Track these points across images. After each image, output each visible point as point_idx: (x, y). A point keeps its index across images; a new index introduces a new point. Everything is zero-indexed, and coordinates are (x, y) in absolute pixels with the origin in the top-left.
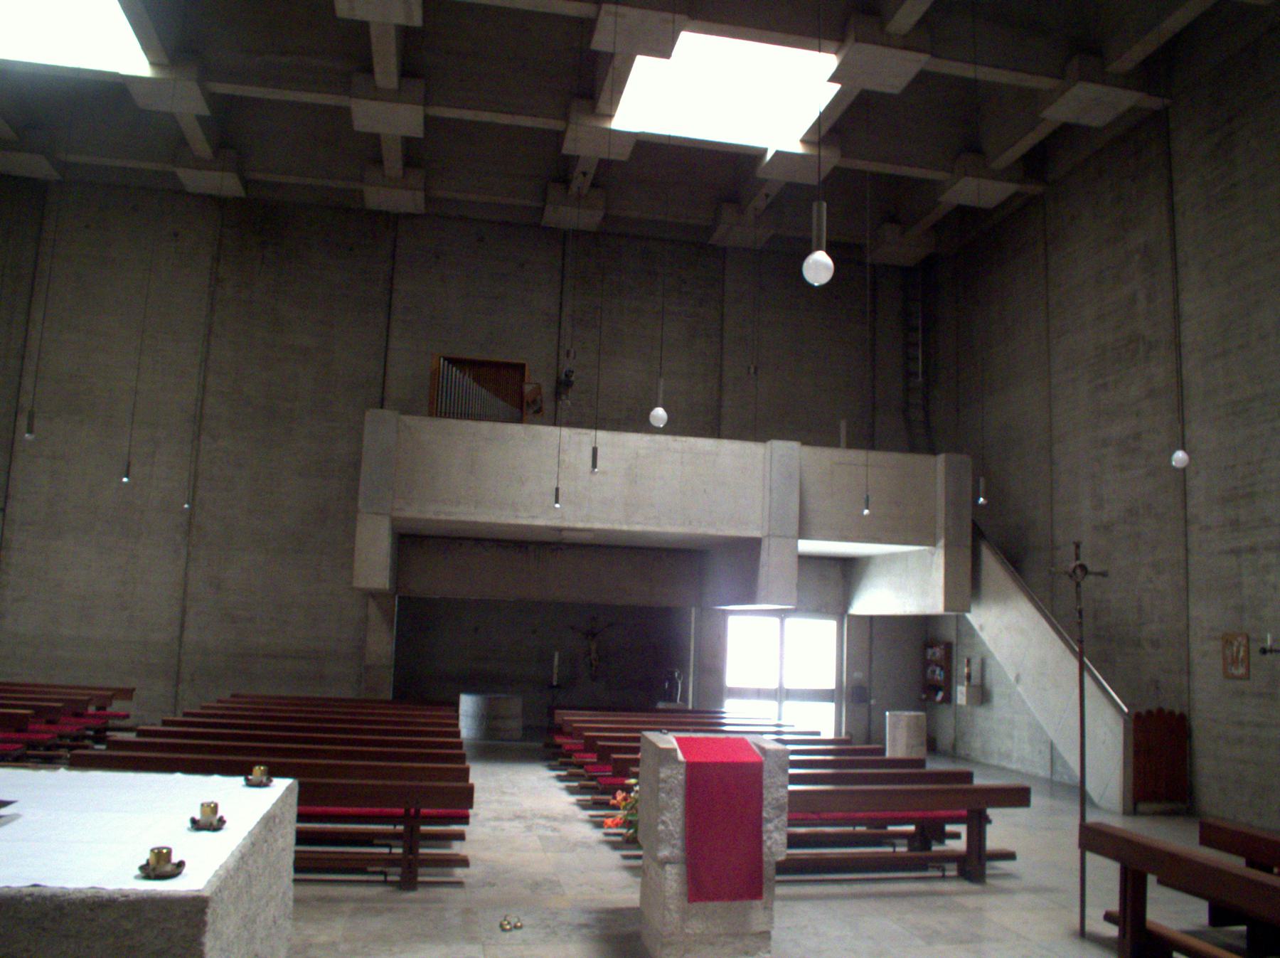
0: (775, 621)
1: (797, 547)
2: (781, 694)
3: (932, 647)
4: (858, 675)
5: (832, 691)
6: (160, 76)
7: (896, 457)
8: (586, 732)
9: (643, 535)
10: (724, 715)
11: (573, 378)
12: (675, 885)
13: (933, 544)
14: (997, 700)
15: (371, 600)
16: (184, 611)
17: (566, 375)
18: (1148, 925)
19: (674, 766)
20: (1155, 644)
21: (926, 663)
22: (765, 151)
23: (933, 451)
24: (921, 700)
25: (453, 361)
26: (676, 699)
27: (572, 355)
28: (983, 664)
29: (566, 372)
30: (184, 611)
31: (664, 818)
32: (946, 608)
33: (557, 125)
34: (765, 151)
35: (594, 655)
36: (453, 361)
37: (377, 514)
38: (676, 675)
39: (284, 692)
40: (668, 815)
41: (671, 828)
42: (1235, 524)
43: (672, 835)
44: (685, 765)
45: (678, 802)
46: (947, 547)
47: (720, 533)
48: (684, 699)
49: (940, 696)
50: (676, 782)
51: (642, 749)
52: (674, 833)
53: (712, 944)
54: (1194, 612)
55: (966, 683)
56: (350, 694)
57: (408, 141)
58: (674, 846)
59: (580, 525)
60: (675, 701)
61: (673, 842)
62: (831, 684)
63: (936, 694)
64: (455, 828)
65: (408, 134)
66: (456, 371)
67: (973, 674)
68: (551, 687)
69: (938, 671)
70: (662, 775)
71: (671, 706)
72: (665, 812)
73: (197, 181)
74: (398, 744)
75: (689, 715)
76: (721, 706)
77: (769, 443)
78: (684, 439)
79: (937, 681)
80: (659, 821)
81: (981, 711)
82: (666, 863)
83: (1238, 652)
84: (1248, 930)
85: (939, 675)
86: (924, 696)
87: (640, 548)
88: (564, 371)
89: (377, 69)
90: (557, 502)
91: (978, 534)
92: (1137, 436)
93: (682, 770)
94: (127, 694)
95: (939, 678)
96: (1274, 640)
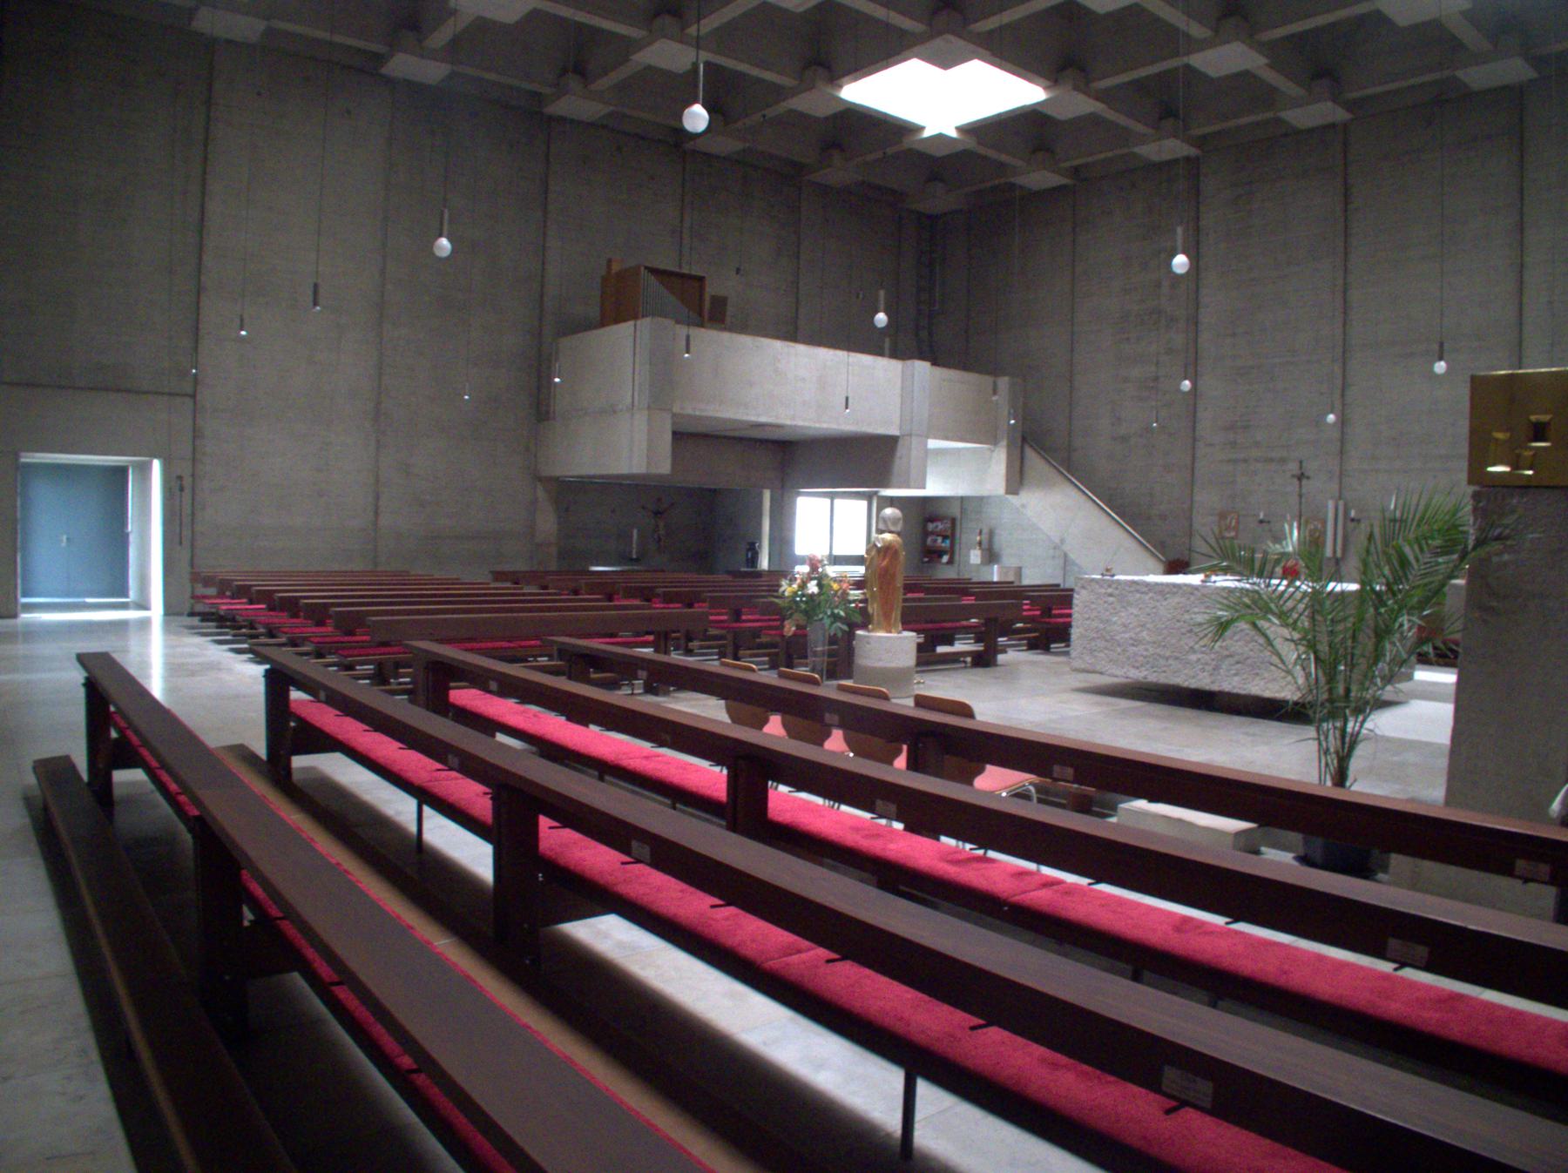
0: (828, 501)
8: (246, 648)
13: (993, 440)
15: (538, 483)
16: (377, 498)
20: (1163, 517)
21: (926, 534)
22: (922, 128)
24: (923, 563)
28: (991, 534)
30: (377, 498)
34: (922, 128)
35: (662, 532)
37: (661, 409)
42: (1233, 444)
49: (945, 559)
51: (901, 601)
54: (1197, 498)
55: (978, 548)
64: (1066, 611)
77: (909, 362)
83: (1231, 522)
84: (1468, 583)
86: (926, 559)
91: (1024, 440)
92: (1156, 379)
96: (1265, 515)
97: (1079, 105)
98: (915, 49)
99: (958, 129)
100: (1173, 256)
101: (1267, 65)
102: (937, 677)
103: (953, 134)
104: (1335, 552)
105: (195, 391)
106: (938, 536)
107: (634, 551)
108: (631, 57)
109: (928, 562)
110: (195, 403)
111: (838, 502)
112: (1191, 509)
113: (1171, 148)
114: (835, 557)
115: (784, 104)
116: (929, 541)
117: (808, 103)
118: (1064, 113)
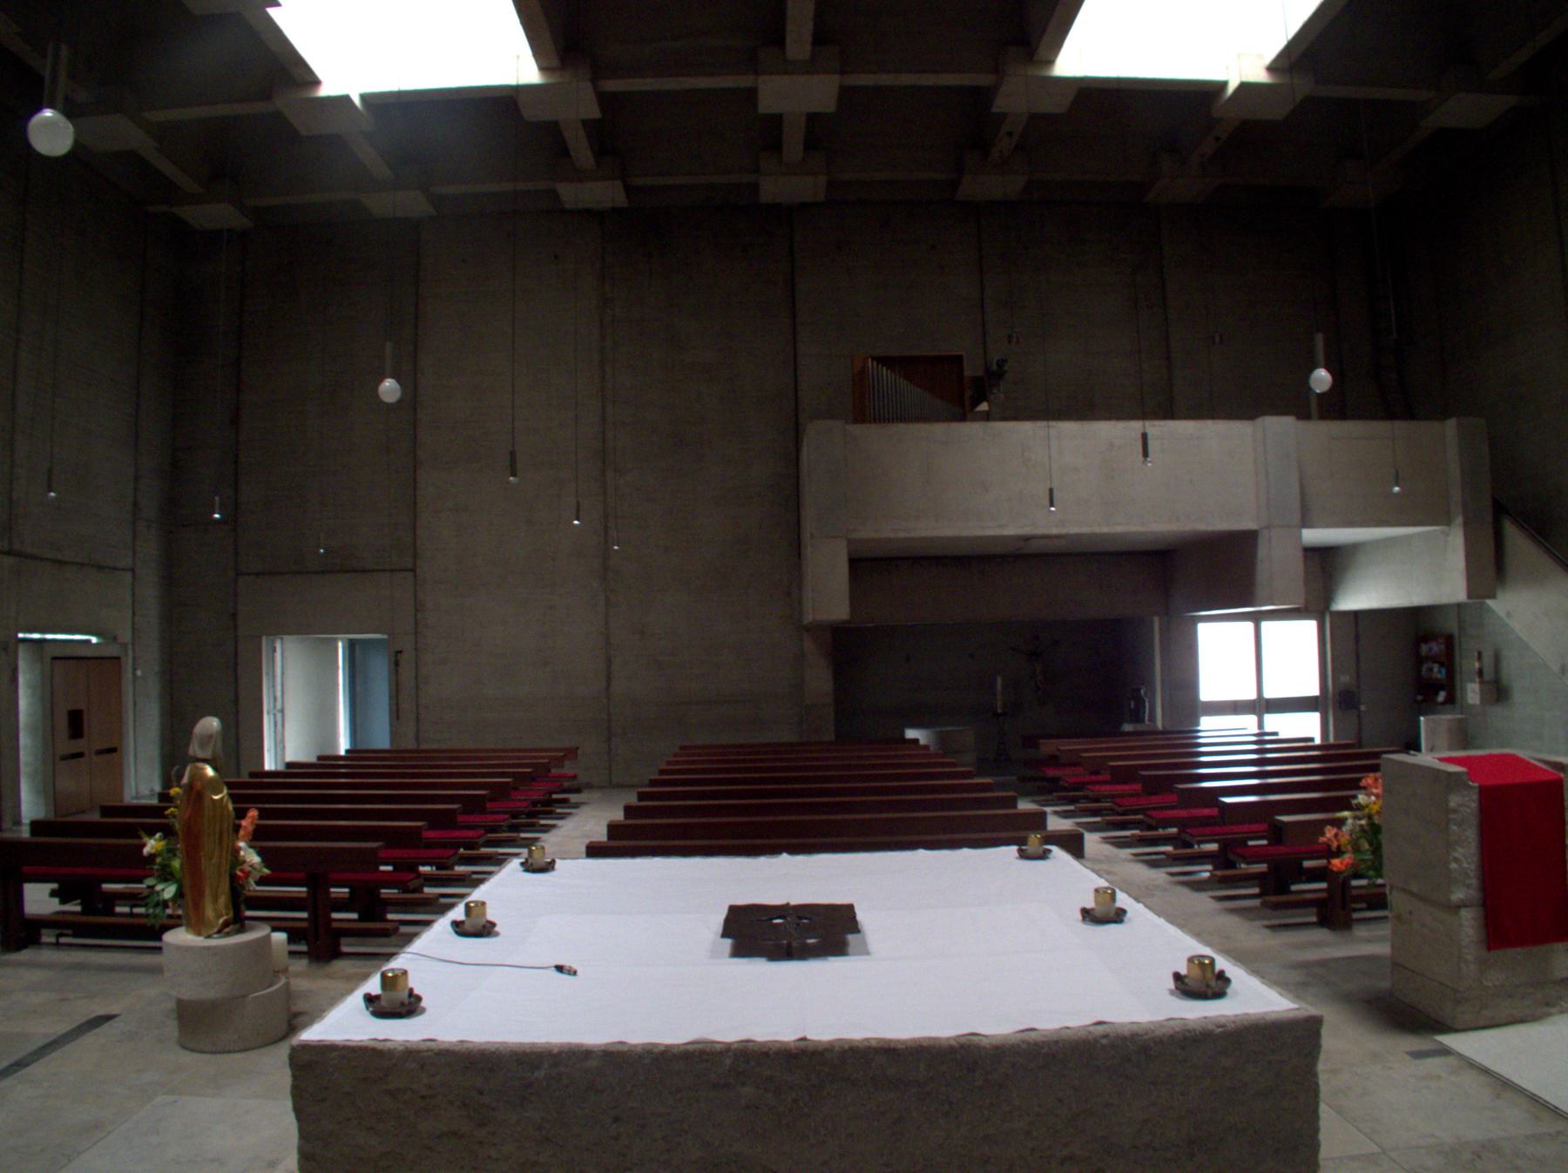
0: (1249, 626)
1: (1300, 537)
2: (1262, 706)
3: (1426, 641)
4: (1345, 679)
5: (1315, 698)
6: (552, 80)
7: (1381, 427)
9: (1079, 536)
10: (1200, 734)
11: (1006, 368)
12: (1471, 932)
13: (1448, 523)
14: (1517, 696)
16: (609, 662)
17: (998, 365)
18: (26, 917)
19: (1465, 792)
21: (1420, 660)
22: (1224, 84)
23: (1441, 413)
24: (1416, 701)
25: (880, 360)
26: (1144, 720)
27: (1015, 340)
28: (1497, 658)
29: (998, 361)
30: (609, 662)
31: (1456, 855)
32: (1469, 597)
33: (984, 80)
36: (880, 360)
38: (1142, 692)
39: (726, 739)
40: (1460, 850)
41: (1465, 865)
43: (1467, 874)
44: (1477, 790)
45: (1471, 834)
46: (1466, 525)
47: (1211, 528)
48: (1152, 718)
49: (1441, 696)
50: (1469, 811)
52: (1469, 872)
53: (1510, 996)
55: (1477, 680)
56: (793, 738)
57: (812, 118)
58: (1468, 887)
59: (1054, 531)
60: (1143, 721)
61: (1468, 882)
62: (1313, 690)
63: (1437, 694)
65: (812, 110)
66: (887, 373)
67: (1485, 671)
68: (996, 715)
69: (1436, 667)
70: (1452, 804)
71: (1140, 727)
72: (1457, 847)
73: (573, 194)
74: (904, 790)
75: (1160, 736)
76: (1198, 724)
78: (1162, 423)
79: (1437, 679)
80: (1451, 858)
81: (1497, 711)
82: (1459, 907)
85: (1438, 673)
86: (1420, 698)
87: (876, 559)
88: (995, 362)
89: (789, 40)
90: (1052, 505)
91: (1499, 510)
93: (1475, 797)
94: (571, 753)
95: (1439, 676)
100: (381, 381)
102: (352, 962)
105: (415, 564)
106: (1435, 662)
107: (999, 704)
109: (1423, 701)
110: (415, 576)
111: (1266, 626)
114: (1268, 701)
116: (1424, 668)
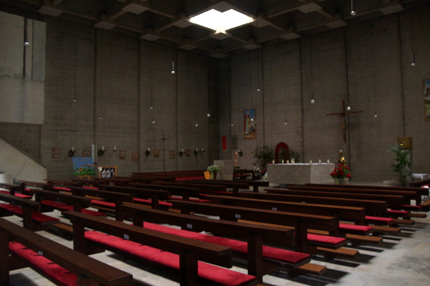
22: (215, 31)
83: (57, 152)
97: (264, 23)
98: (213, 6)
99: (226, 31)
101: (322, 9)
103: (224, 32)
104: (95, 161)
108: (123, 9)
112: (40, 147)
113: (292, 36)
115: (171, 24)
117: (180, 24)
118: (260, 26)
